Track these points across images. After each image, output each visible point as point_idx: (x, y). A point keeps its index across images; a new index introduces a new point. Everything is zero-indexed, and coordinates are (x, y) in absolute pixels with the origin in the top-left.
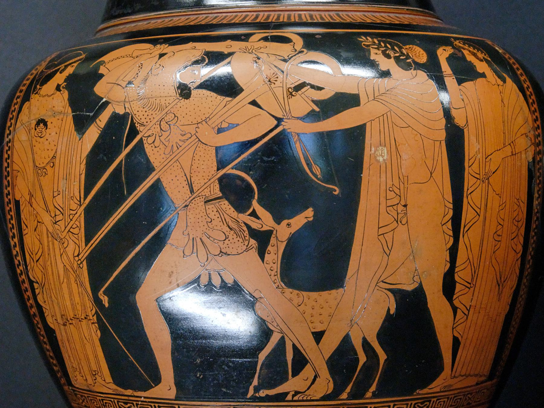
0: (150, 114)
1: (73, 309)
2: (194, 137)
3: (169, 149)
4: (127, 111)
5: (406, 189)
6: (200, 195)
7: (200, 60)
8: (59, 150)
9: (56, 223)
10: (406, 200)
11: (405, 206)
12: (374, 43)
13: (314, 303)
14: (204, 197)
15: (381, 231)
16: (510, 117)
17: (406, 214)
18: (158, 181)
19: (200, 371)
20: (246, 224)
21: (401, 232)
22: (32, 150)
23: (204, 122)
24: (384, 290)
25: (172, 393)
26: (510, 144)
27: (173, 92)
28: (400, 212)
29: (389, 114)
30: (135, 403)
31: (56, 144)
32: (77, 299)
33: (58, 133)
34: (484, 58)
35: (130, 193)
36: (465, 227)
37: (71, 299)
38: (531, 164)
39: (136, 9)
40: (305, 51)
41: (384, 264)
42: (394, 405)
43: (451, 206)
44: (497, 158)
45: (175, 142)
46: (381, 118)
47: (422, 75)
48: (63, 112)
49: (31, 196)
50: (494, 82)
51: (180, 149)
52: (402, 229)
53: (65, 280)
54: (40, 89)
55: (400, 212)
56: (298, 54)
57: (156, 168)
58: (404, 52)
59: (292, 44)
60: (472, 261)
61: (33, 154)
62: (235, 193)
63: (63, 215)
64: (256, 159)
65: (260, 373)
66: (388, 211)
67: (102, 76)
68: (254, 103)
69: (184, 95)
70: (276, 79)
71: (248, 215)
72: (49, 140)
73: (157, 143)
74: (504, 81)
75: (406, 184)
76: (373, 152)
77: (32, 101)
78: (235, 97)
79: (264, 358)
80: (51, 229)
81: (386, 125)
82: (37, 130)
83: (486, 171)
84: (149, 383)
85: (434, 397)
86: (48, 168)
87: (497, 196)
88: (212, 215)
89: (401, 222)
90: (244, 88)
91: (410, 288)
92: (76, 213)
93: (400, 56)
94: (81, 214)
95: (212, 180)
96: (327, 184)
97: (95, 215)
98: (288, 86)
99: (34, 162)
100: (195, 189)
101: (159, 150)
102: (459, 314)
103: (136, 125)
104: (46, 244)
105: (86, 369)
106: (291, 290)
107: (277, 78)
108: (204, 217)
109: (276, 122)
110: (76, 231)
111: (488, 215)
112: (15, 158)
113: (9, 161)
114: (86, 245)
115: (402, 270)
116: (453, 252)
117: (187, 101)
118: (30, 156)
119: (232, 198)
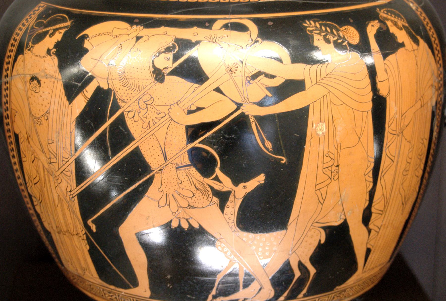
0: (130, 93)
1: (67, 226)
2: (167, 116)
3: (146, 125)
4: (110, 87)
5: (339, 154)
6: (172, 162)
7: (171, 47)
9: (51, 163)
10: (338, 162)
11: (338, 166)
14: (176, 164)
15: (318, 187)
17: (338, 172)
19: (169, 283)
20: (209, 185)
21: (334, 186)
23: (176, 105)
24: (317, 228)
25: (148, 293)
26: (420, 99)
27: (149, 76)
28: (333, 170)
31: (49, 102)
32: (69, 221)
33: (51, 94)
34: (403, 26)
37: (64, 219)
38: (435, 107)
42: (319, 299)
45: (151, 119)
46: (322, 99)
48: (54, 76)
51: (156, 125)
52: (334, 184)
53: (59, 205)
54: (32, 47)
55: (333, 170)
56: (254, 43)
57: (135, 138)
58: (341, 34)
59: (249, 32)
60: (385, 196)
62: (202, 163)
63: (57, 159)
64: (219, 137)
66: (324, 172)
68: (218, 90)
69: (159, 80)
70: (236, 69)
71: (212, 179)
72: (43, 97)
73: (136, 118)
75: (339, 149)
76: (314, 128)
78: (202, 85)
80: (46, 166)
81: (326, 105)
82: (32, 85)
83: (401, 127)
86: (43, 119)
87: (408, 143)
88: (182, 178)
89: (334, 179)
90: (209, 76)
92: (68, 161)
93: (338, 40)
94: (72, 162)
95: (183, 152)
96: (276, 155)
98: (246, 75)
99: (30, 110)
100: (168, 158)
101: (138, 124)
102: (373, 233)
103: (118, 100)
107: (237, 67)
108: (175, 179)
110: (68, 174)
113: (8, 105)
114: (77, 186)
115: (332, 212)
116: (372, 194)
117: (161, 85)
118: (26, 104)
119: (199, 166)
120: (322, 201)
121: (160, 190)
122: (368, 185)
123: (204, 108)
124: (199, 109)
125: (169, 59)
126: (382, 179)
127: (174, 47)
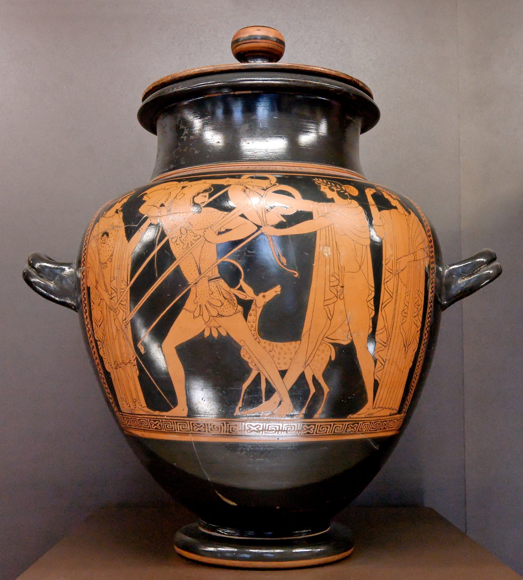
1: (122, 357)
3: (186, 246)
8: (115, 250)
9: (111, 299)
11: (342, 287)
12: (324, 182)
13: (281, 351)
15: (326, 303)
16: (413, 236)
17: (343, 292)
18: (178, 266)
22: (99, 252)
23: (209, 228)
29: (332, 226)
30: (160, 420)
32: (124, 350)
35: (159, 275)
36: (382, 304)
37: (120, 350)
38: (427, 269)
39: (171, 168)
40: (278, 184)
41: (328, 325)
43: (373, 289)
44: (404, 262)
46: (327, 228)
47: (355, 203)
49: (97, 282)
50: (403, 213)
51: (193, 245)
52: (340, 303)
55: (339, 291)
61: (99, 255)
65: (243, 398)
67: (145, 201)
68: (242, 216)
73: (178, 242)
74: (410, 213)
77: (100, 222)
79: (246, 388)
80: (108, 303)
81: (330, 233)
84: (169, 406)
85: (362, 421)
86: (108, 262)
91: (345, 343)
95: (214, 266)
97: (136, 292)
100: (202, 272)
102: (378, 364)
104: (105, 313)
105: (129, 398)
106: (265, 341)
109: (256, 228)
110: (124, 303)
111: (398, 298)
112: (89, 260)
115: (340, 330)
116: (375, 321)
118: (97, 256)
120: (330, 317)
121: (195, 302)
122: (370, 312)
123: (231, 230)
124: (227, 230)
125: (205, 196)
126: (383, 310)
127: (210, 189)
